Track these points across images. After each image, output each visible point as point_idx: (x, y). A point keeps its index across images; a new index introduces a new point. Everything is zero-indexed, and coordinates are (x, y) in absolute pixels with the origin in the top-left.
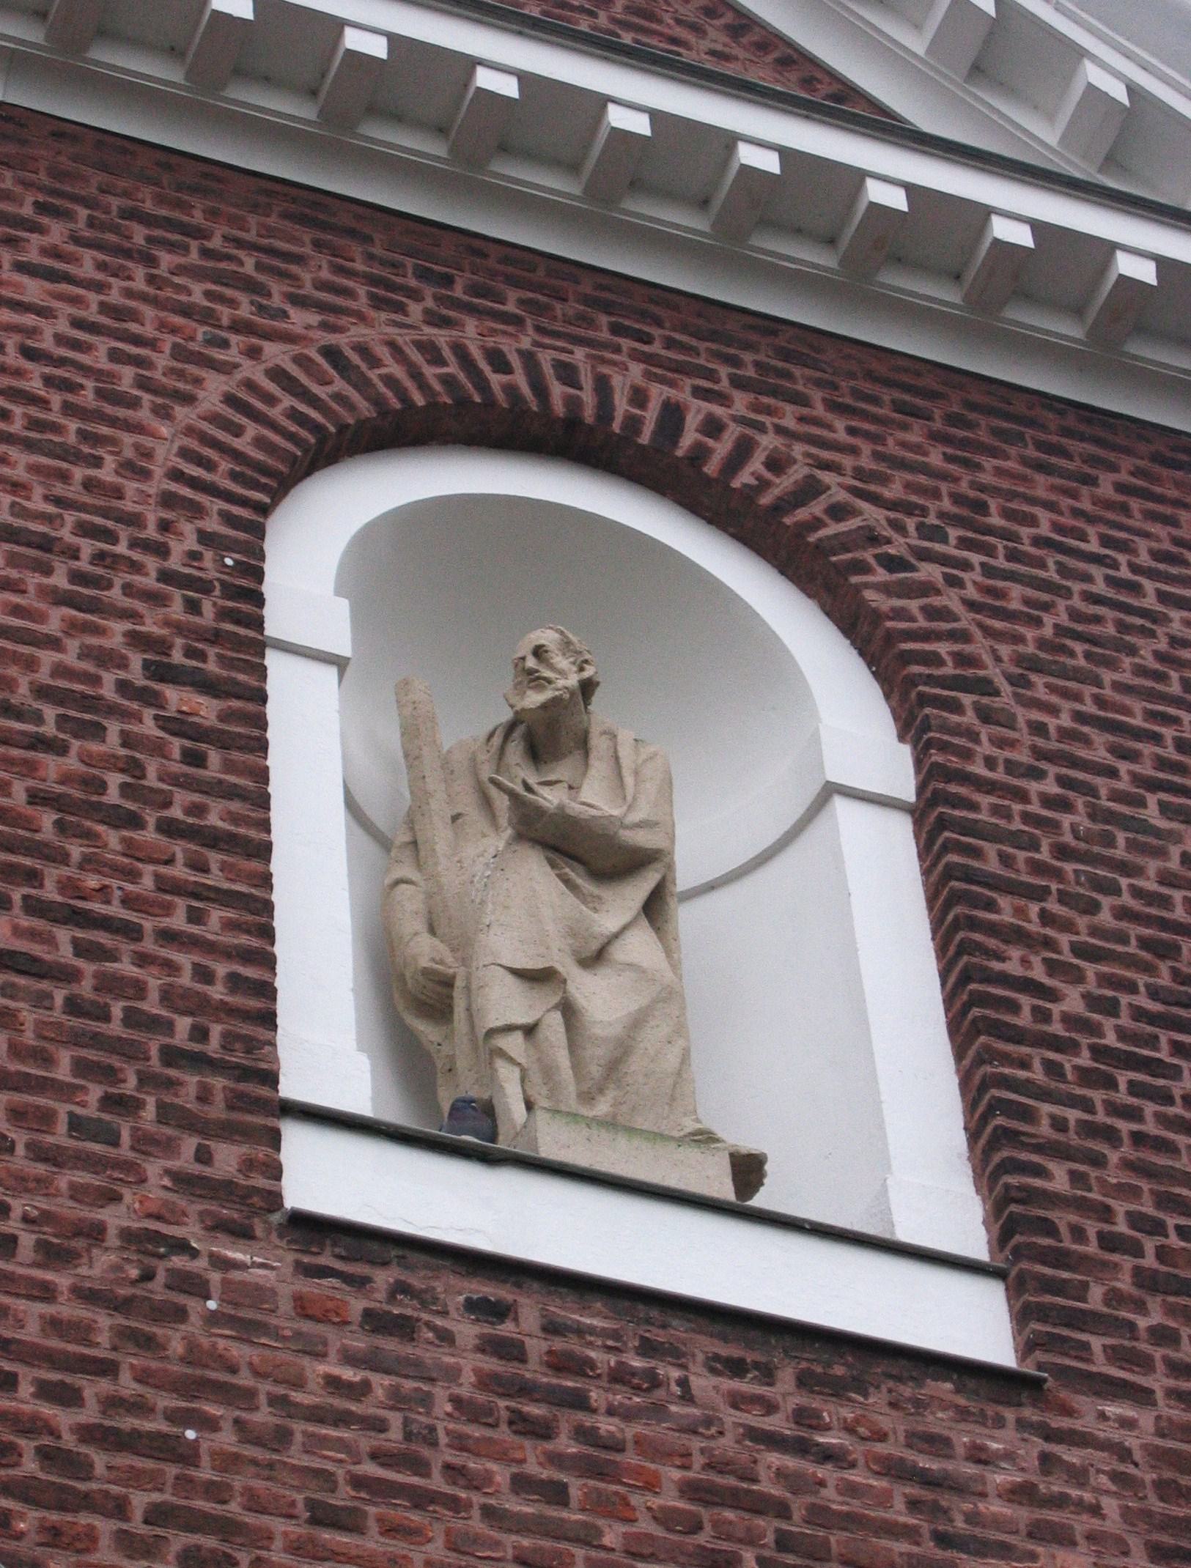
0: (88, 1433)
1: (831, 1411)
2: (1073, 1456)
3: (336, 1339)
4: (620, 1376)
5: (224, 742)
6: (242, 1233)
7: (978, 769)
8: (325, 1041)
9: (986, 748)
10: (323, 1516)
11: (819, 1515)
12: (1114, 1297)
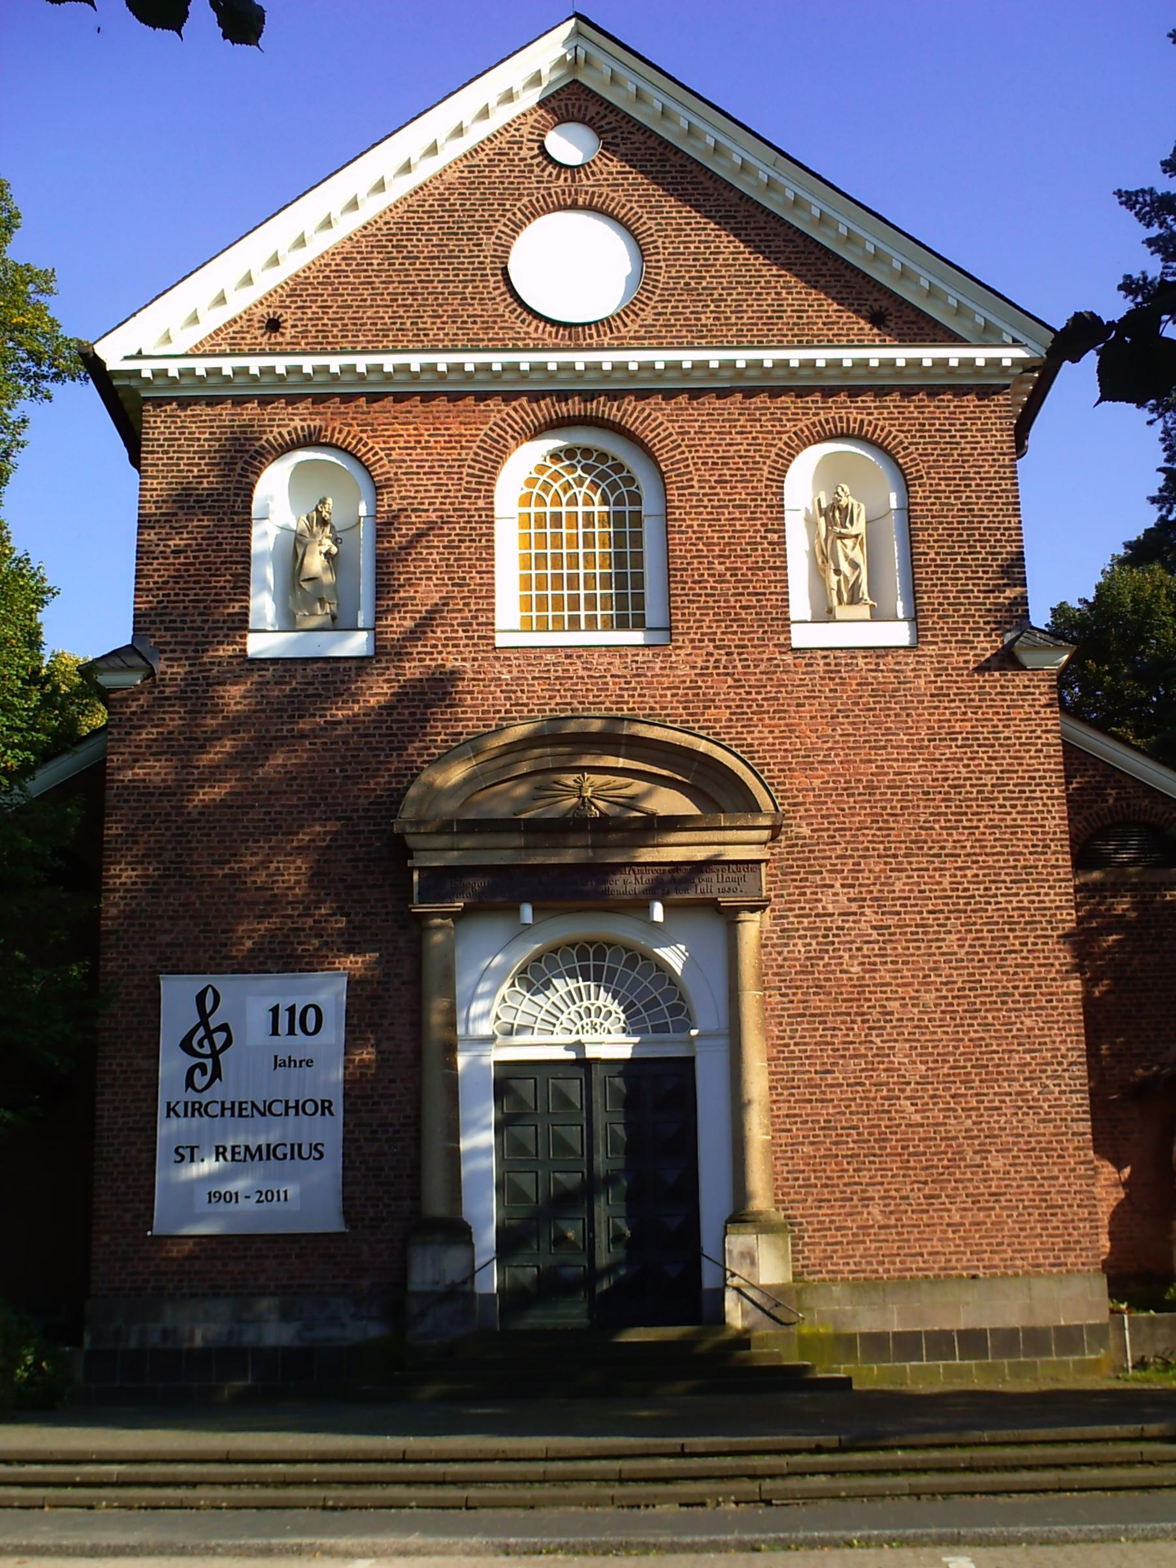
0: (763, 699)
1: (881, 661)
2: (922, 659)
3: (800, 670)
4: (847, 665)
5: (778, 544)
6: (785, 653)
7: (918, 500)
8: (800, 604)
9: (921, 494)
10: (798, 705)
11: (879, 683)
12: (933, 623)
